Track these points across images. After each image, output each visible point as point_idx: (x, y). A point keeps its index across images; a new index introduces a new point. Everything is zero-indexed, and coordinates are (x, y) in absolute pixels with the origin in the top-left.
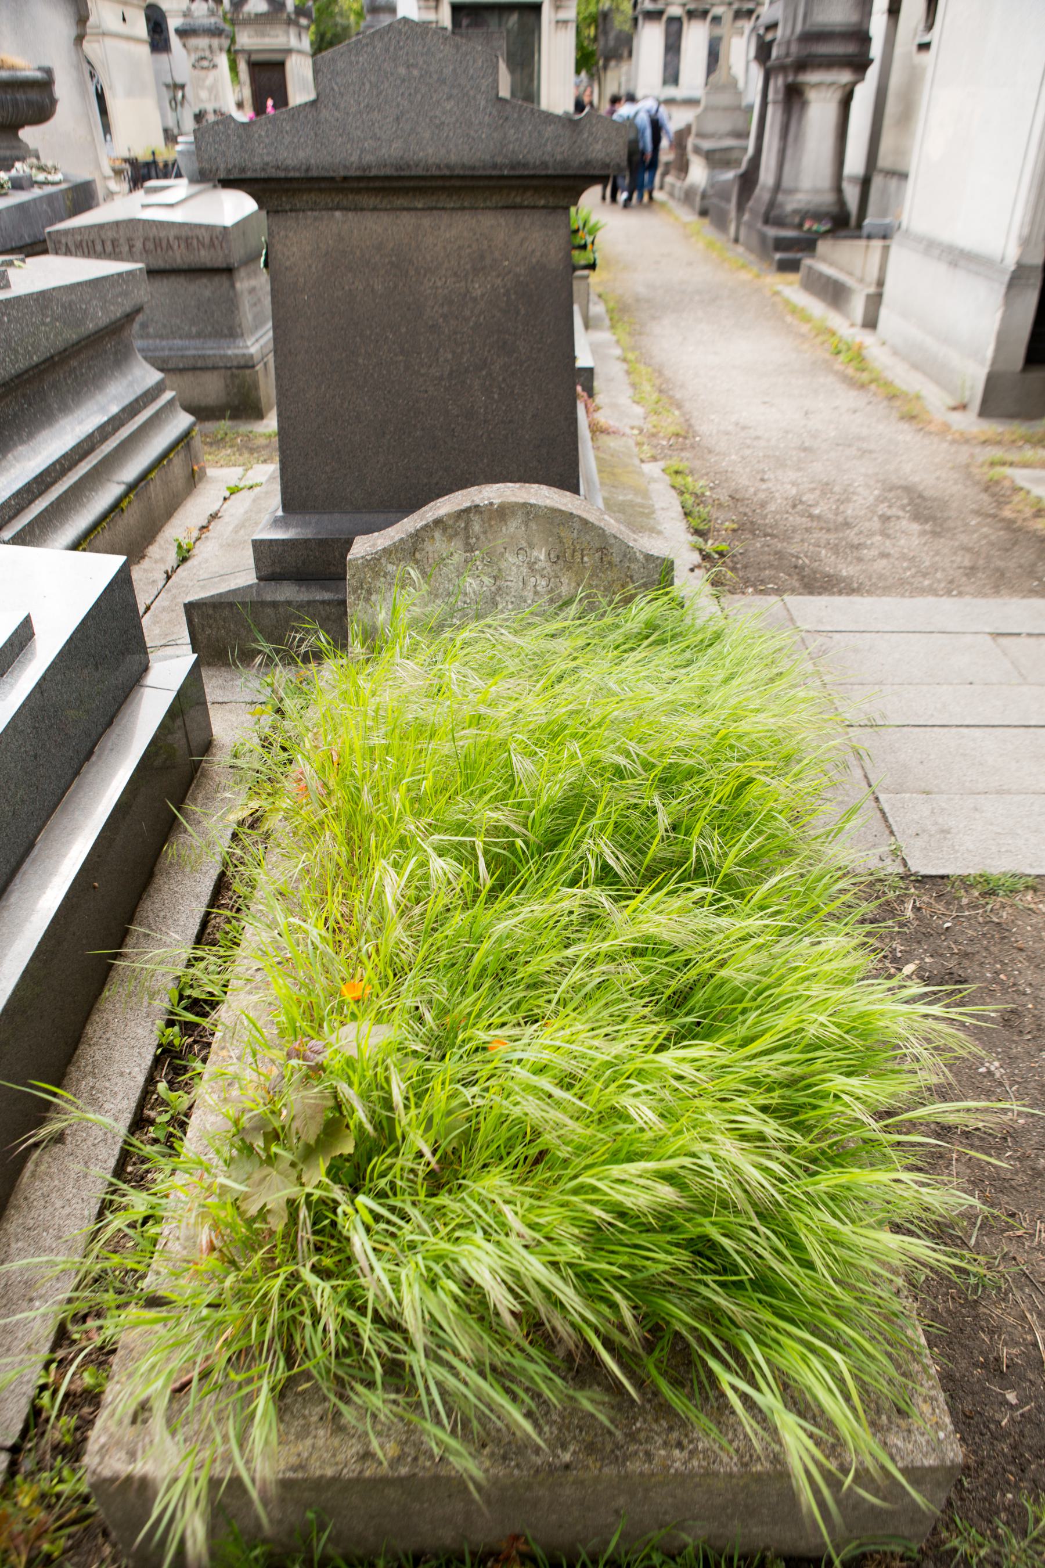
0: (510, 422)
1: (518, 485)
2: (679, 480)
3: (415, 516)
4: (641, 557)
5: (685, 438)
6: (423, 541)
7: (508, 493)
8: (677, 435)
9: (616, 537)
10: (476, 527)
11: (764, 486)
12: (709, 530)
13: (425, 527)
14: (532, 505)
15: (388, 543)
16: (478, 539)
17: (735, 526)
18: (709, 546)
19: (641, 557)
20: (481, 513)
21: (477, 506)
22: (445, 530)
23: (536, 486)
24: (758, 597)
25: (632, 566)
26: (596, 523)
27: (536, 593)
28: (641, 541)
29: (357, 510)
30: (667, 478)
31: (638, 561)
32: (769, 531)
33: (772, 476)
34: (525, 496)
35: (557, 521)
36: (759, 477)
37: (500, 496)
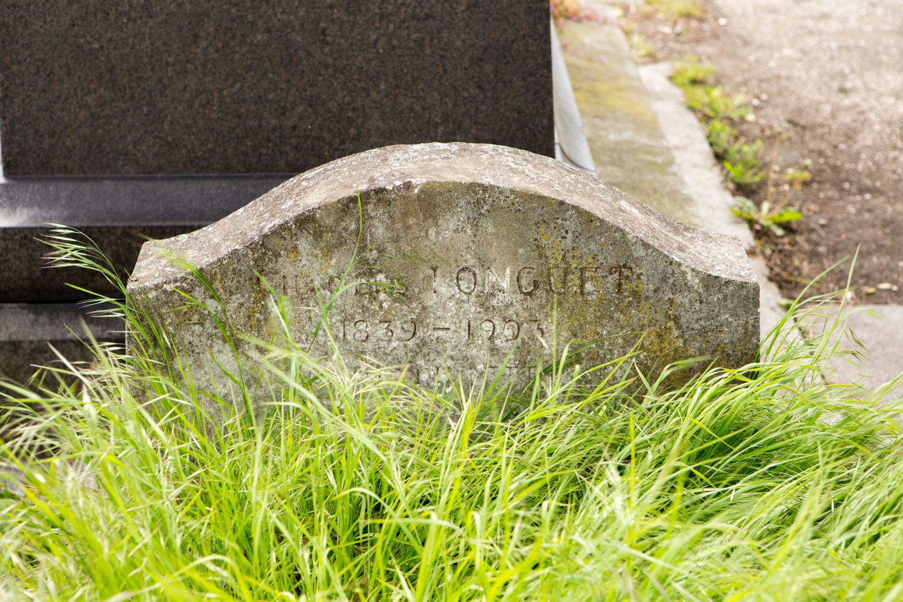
0: (428, 16)
1: (455, 146)
2: (699, 93)
3: (258, 205)
4: (695, 282)
5: (701, 20)
6: (277, 255)
7: (439, 164)
8: (688, 16)
9: (646, 246)
10: (380, 231)
11: (847, 102)
12: (763, 183)
13: (281, 231)
14: (485, 188)
15: (206, 260)
16: (381, 251)
17: (806, 175)
18: (765, 215)
19: (695, 282)
20: (388, 203)
21: (380, 191)
22: (318, 235)
23: (489, 147)
24: (865, 310)
25: (679, 299)
26: (610, 219)
27: (494, 350)
28: (692, 248)
29: (148, 174)
30: (678, 92)
31: (689, 288)
32: (868, 182)
33: (859, 84)
34: (471, 168)
35: (534, 217)
36: (835, 85)
37: (424, 171)
